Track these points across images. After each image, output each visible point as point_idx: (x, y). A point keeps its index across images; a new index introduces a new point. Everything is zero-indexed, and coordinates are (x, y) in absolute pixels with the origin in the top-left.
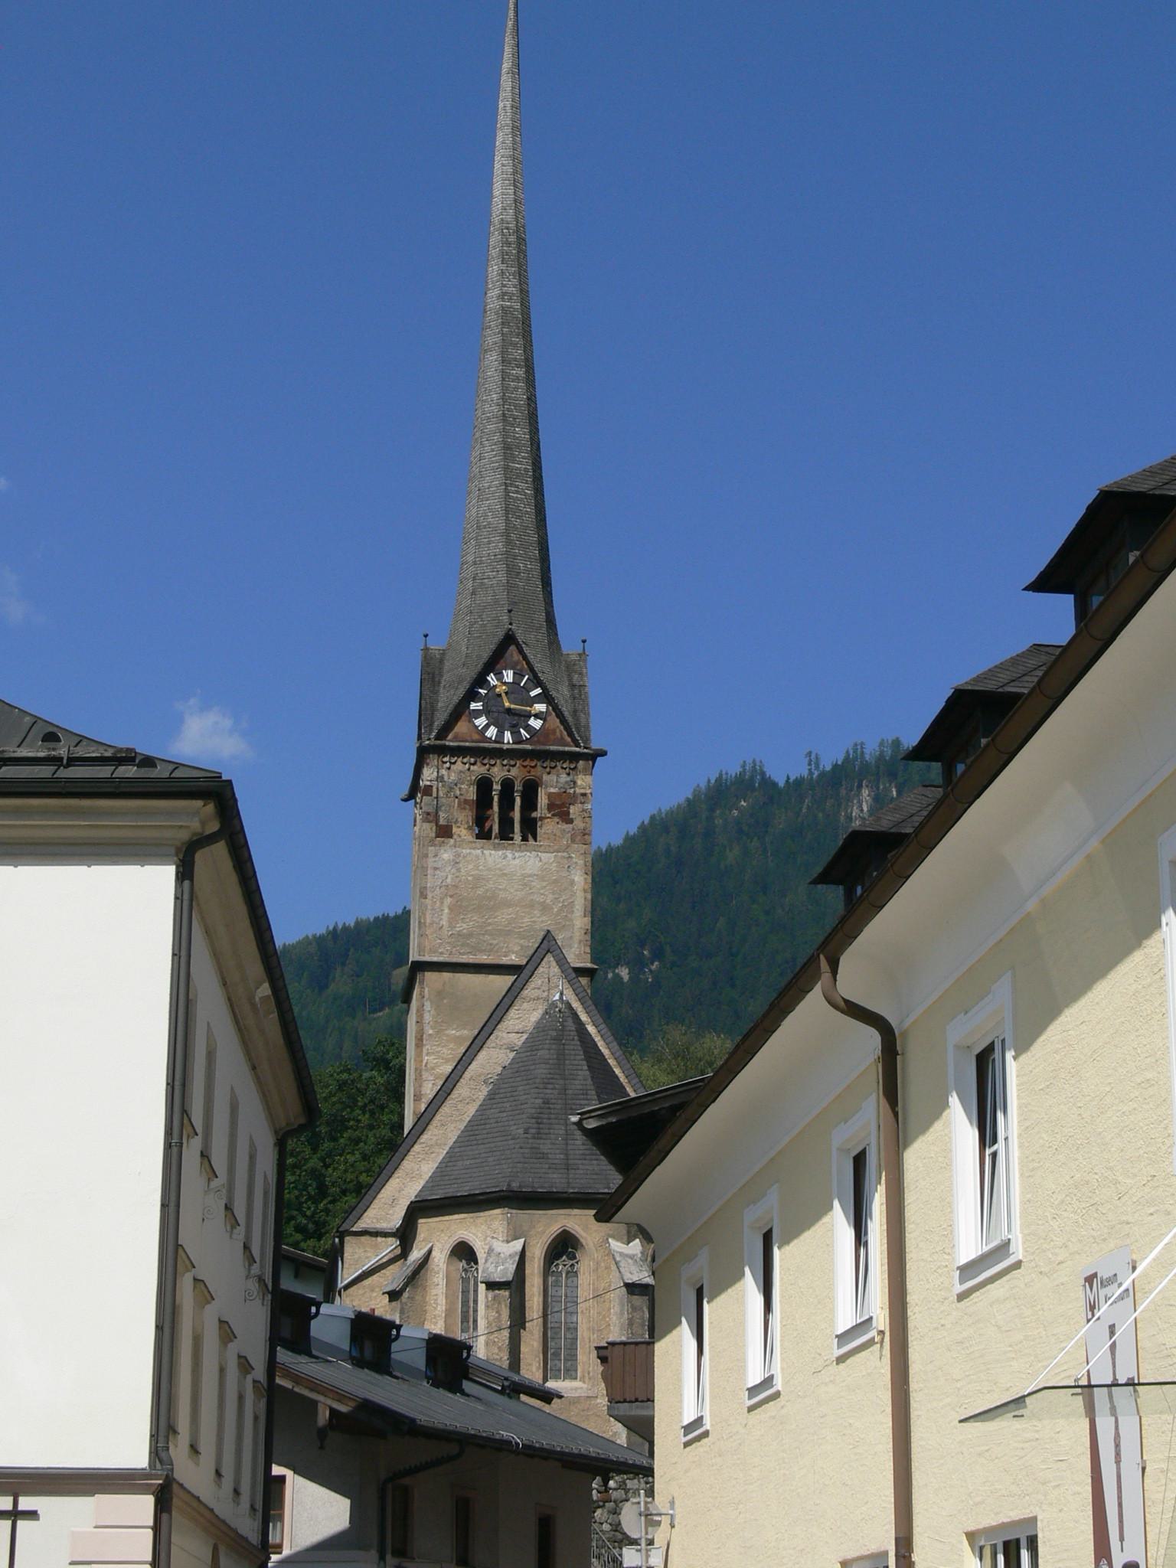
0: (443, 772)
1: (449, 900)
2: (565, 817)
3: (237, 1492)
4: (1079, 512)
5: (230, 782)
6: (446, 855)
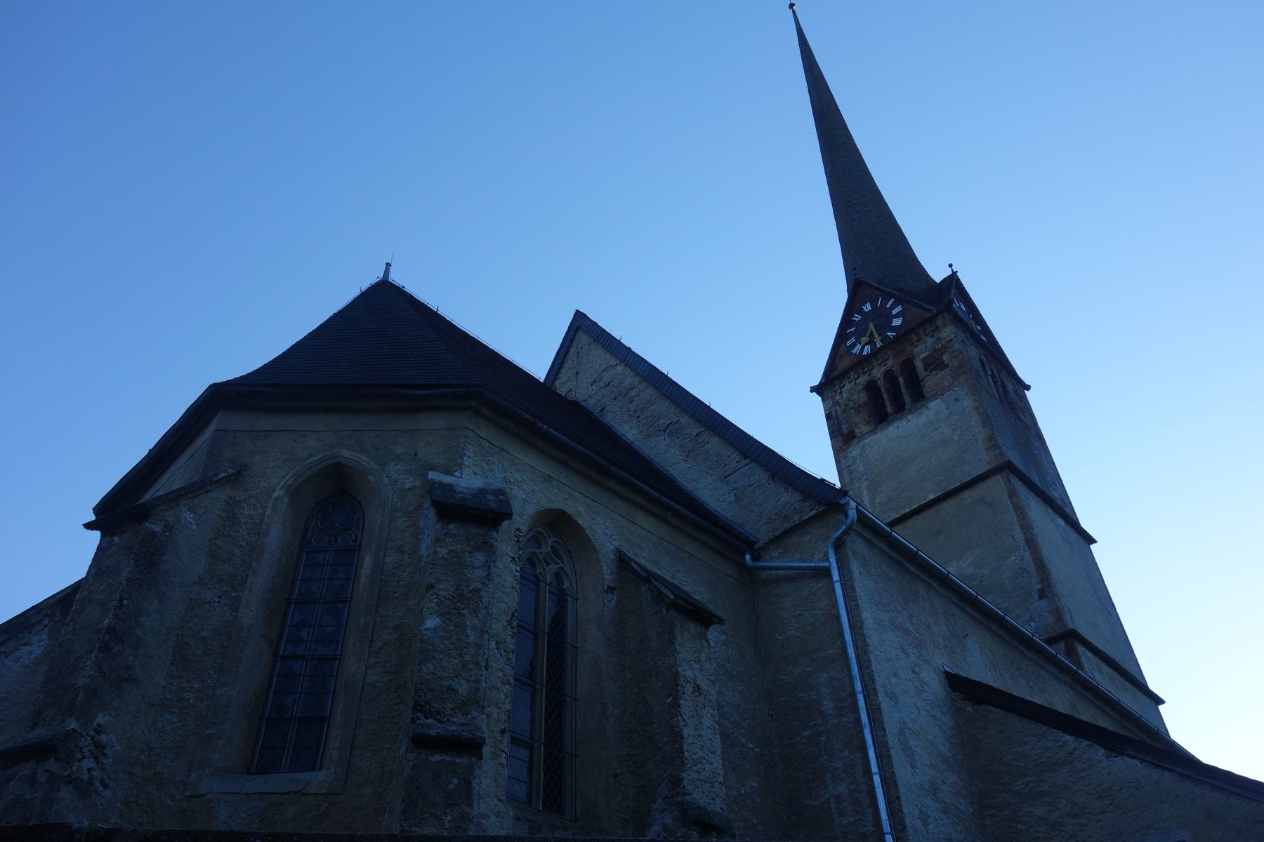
2: (942, 366)
3: (906, 748)
4: (331, 314)
5: (953, 281)
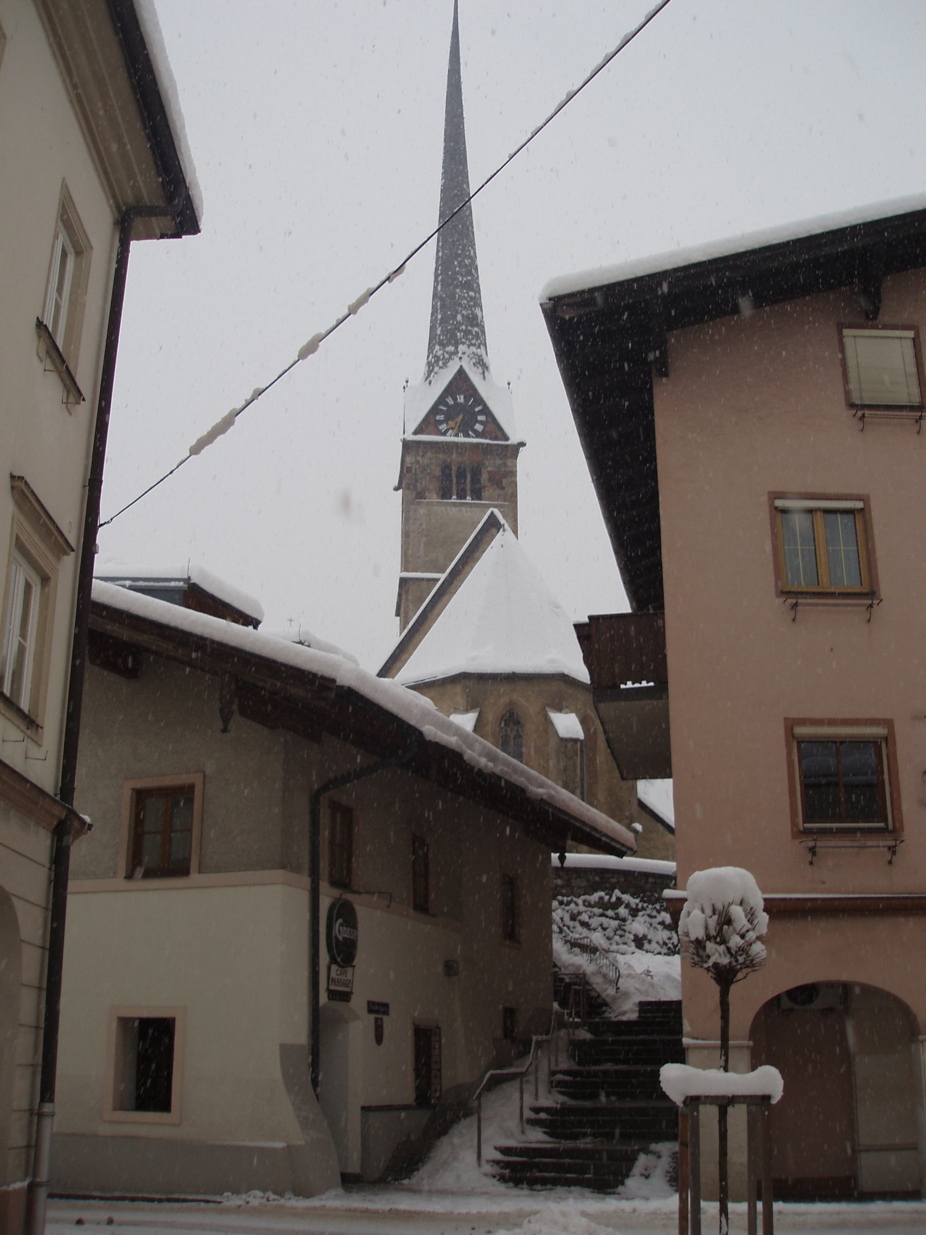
0: (419, 458)
1: (424, 539)
5: (590, 618)
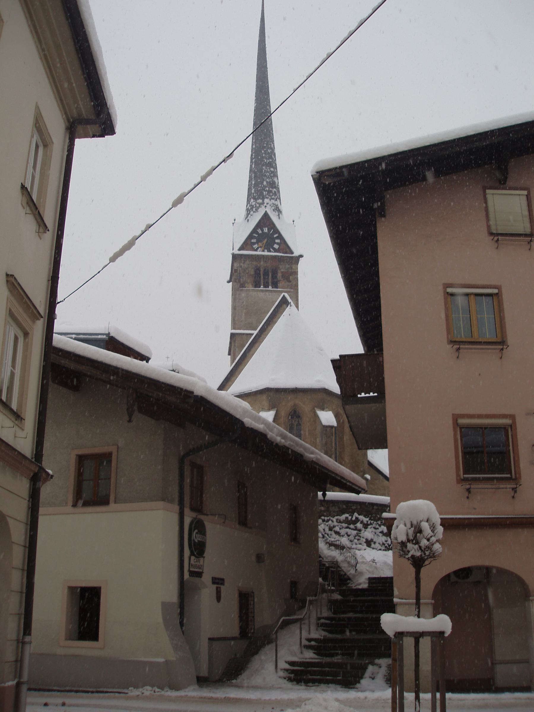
1: (245, 311)
5: (340, 356)
6: (243, 295)
